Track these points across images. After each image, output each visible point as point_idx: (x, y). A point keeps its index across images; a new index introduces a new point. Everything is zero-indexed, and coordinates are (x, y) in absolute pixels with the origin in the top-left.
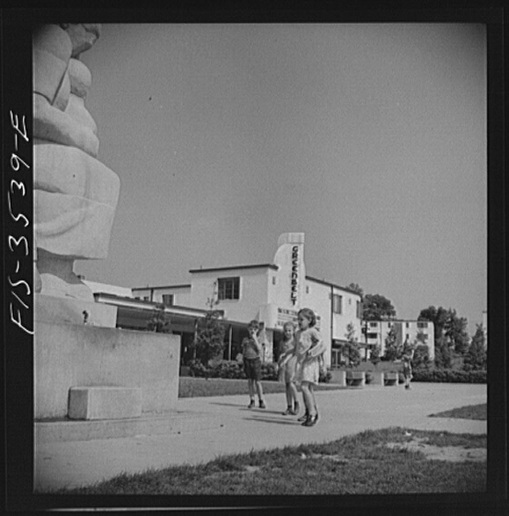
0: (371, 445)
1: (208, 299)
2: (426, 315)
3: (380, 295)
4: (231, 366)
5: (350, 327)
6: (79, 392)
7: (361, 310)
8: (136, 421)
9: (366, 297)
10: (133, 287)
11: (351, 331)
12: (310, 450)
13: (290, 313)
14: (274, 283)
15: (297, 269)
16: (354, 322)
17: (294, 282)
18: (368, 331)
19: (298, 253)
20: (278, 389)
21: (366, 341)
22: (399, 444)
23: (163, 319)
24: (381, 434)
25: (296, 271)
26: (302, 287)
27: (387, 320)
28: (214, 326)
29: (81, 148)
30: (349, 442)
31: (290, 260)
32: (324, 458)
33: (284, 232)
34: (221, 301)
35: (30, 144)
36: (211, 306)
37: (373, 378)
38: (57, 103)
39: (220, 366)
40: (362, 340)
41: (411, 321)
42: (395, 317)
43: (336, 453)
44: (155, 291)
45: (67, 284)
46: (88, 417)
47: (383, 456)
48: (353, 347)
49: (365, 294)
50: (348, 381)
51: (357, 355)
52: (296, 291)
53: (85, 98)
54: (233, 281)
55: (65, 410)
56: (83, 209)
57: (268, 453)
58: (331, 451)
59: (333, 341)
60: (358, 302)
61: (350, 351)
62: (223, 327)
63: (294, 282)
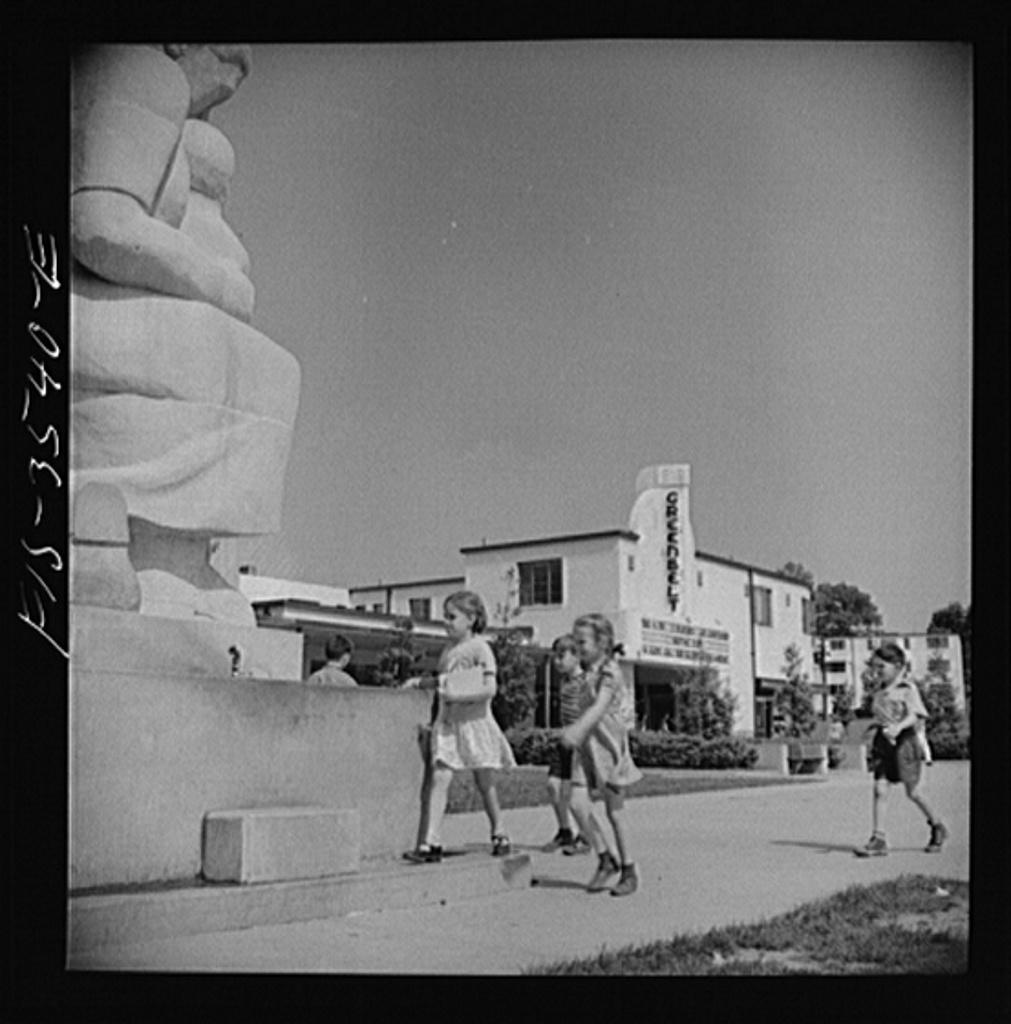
0: (865, 921)
1: (499, 605)
2: (945, 620)
3: (849, 584)
4: (550, 740)
5: (790, 653)
6: (223, 822)
7: (812, 617)
8: (353, 881)
9: (820, 588)
10: (353, 586)
11: (795, 660)
12: (732, 943)
13: (668, 627)
14: (631, 568)
15: (677, 538)
16: (799, 644)
17: (672, 565)
18: (828, 659)
19: (678, 505)
20: (649, 789)
21: (824, 679)
22: (925, 917)
23: (408, 647)
24: (884, 894)
25: (676, 542)
26: (688, 574)
27: (865, 635)
28: (511, 662)
29: (217, 303)
30: (815, 918)
31: (663, 520)
32: (764, 960)
33: (649, 464)
34: (525, 608)
35: (64, 291)
36: (505, 620)
37: (844, 754)
38: (163, 213)
39: (529, 740)
40: (816, 677)
41: (914, 635)
42: (881, 628)
43: (787, 945)
44: (395, 593)
45: (197, 591)
46: (243, 878)
47: (897, 955)
48: (799, 694)
49: (816, 583)
50: (792, 763)
51: (808, 708)
52: (677, 583)
53: (222, 199)
54: (548, 565)
55: (194, 863)
56: (225, 433)
57: (638, 954)
58: (777, 942)
59: (758, 681)
60: (804, 601)
61: (795, 701)
62: (532, 663)
63: (672, 565)
